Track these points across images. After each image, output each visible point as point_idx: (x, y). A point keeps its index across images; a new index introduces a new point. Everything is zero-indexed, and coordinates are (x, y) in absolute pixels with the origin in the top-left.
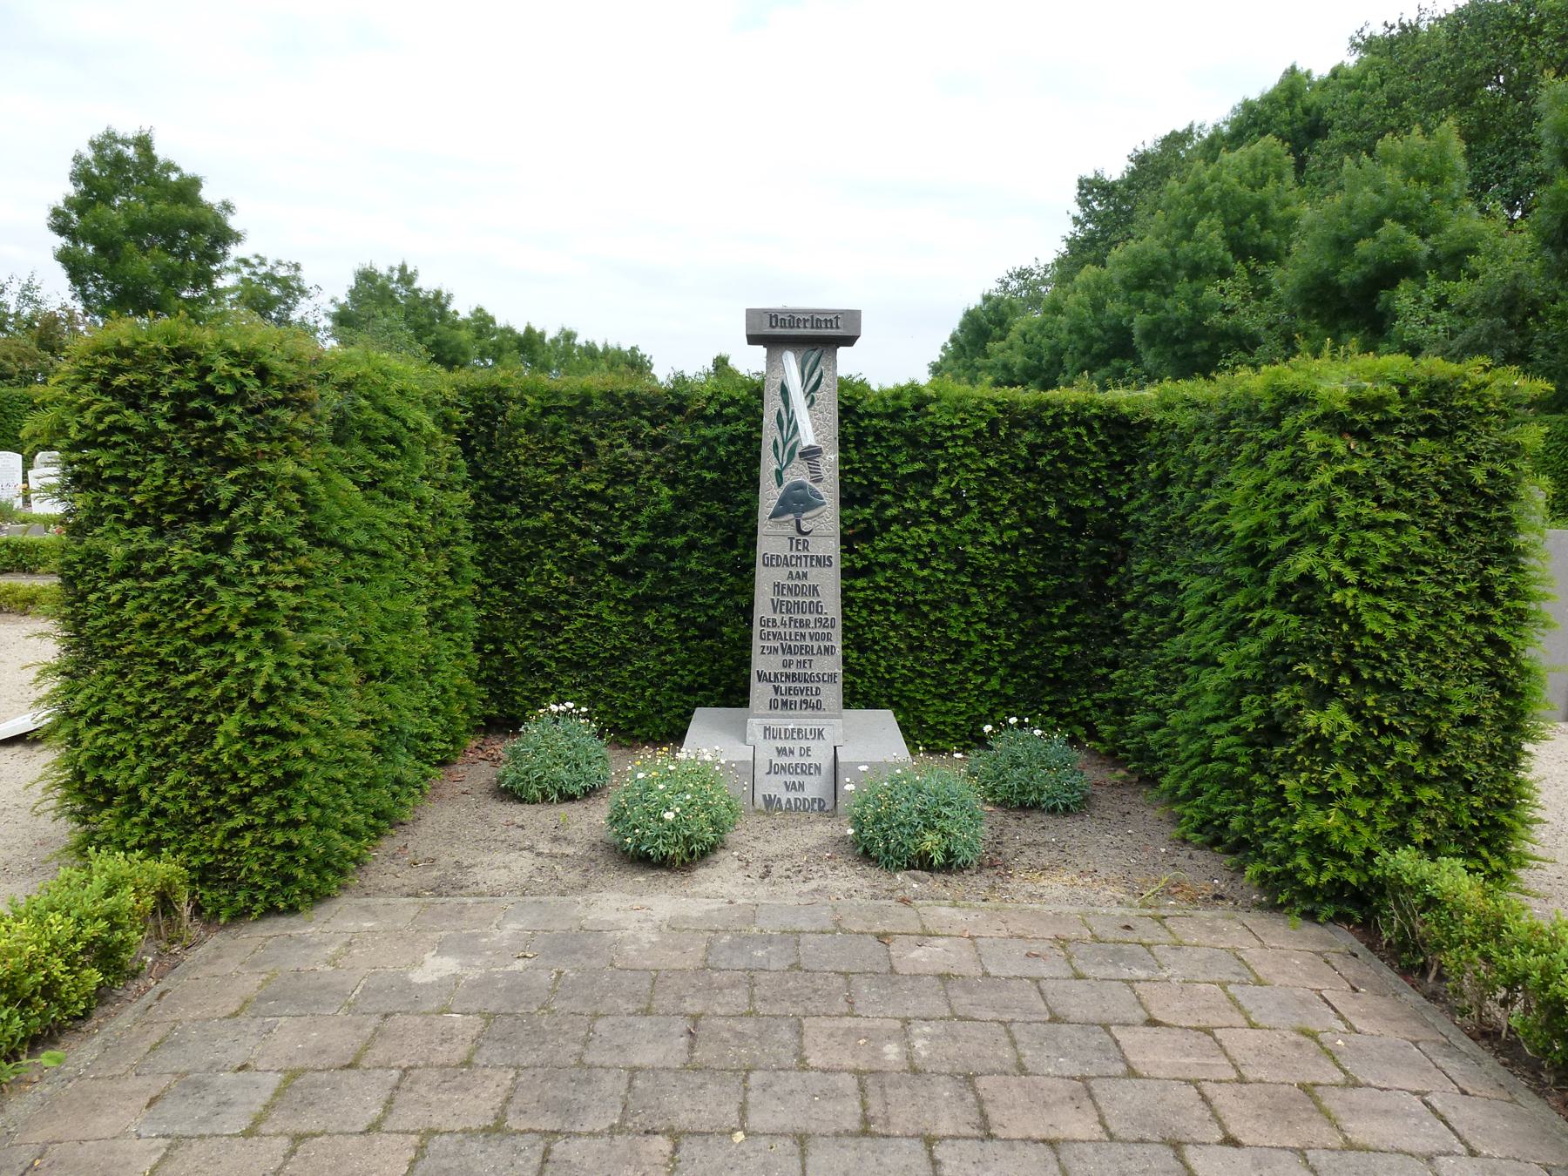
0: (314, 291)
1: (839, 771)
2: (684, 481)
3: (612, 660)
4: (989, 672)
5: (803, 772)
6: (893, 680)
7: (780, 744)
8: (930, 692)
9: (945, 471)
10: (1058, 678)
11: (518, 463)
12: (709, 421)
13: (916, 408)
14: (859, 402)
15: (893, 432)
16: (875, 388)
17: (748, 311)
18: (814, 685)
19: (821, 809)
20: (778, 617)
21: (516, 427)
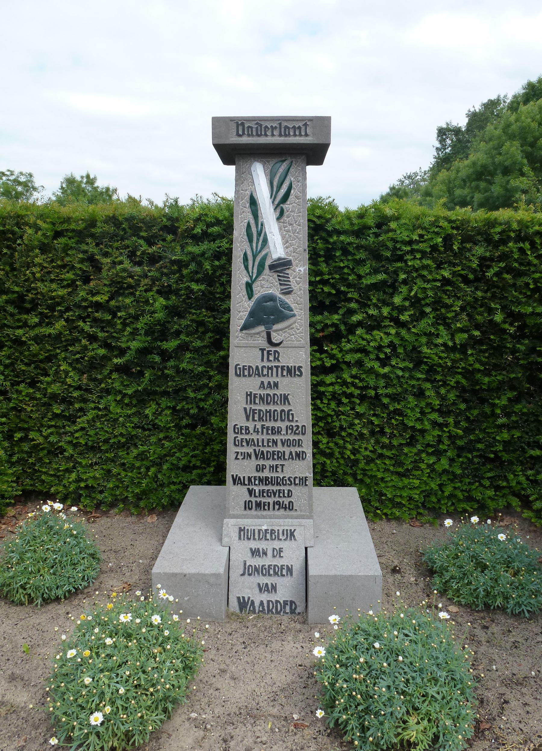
0: (40, 188)
1: (310, 583)
2: (176, 293)
3: (121, 446)
4: (438, 454)
5: (276, 574)
6: (357, 461)
7: (254, 545)
8: (388, 470)
9: (405, 282)
10: (497, 458)
11: (36, 279)
12: (197, 239)
13: (379, 226)
14: (328, 221)
15: (359, 247)
16: (342, 209)
17: (213, 118)
18: (286, 488)
19: (293, 612)
20: (251, 425)
21: (32, 249)
